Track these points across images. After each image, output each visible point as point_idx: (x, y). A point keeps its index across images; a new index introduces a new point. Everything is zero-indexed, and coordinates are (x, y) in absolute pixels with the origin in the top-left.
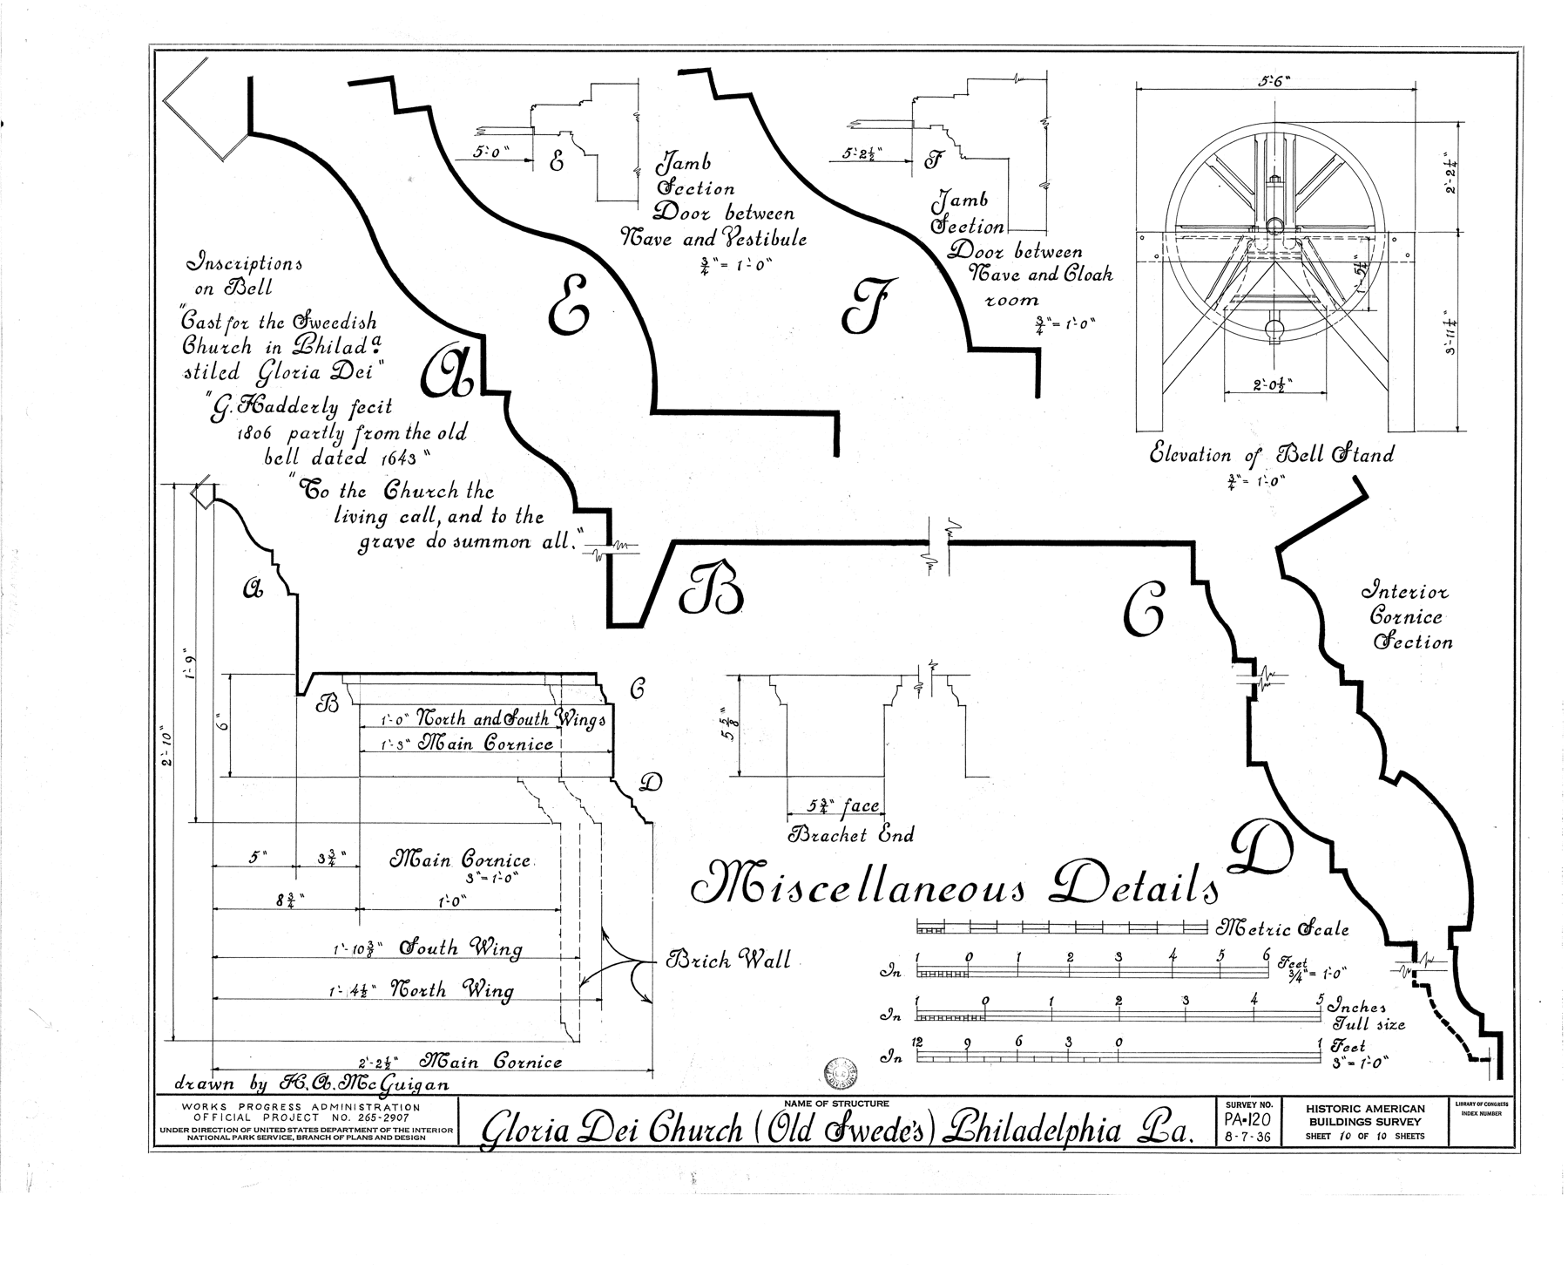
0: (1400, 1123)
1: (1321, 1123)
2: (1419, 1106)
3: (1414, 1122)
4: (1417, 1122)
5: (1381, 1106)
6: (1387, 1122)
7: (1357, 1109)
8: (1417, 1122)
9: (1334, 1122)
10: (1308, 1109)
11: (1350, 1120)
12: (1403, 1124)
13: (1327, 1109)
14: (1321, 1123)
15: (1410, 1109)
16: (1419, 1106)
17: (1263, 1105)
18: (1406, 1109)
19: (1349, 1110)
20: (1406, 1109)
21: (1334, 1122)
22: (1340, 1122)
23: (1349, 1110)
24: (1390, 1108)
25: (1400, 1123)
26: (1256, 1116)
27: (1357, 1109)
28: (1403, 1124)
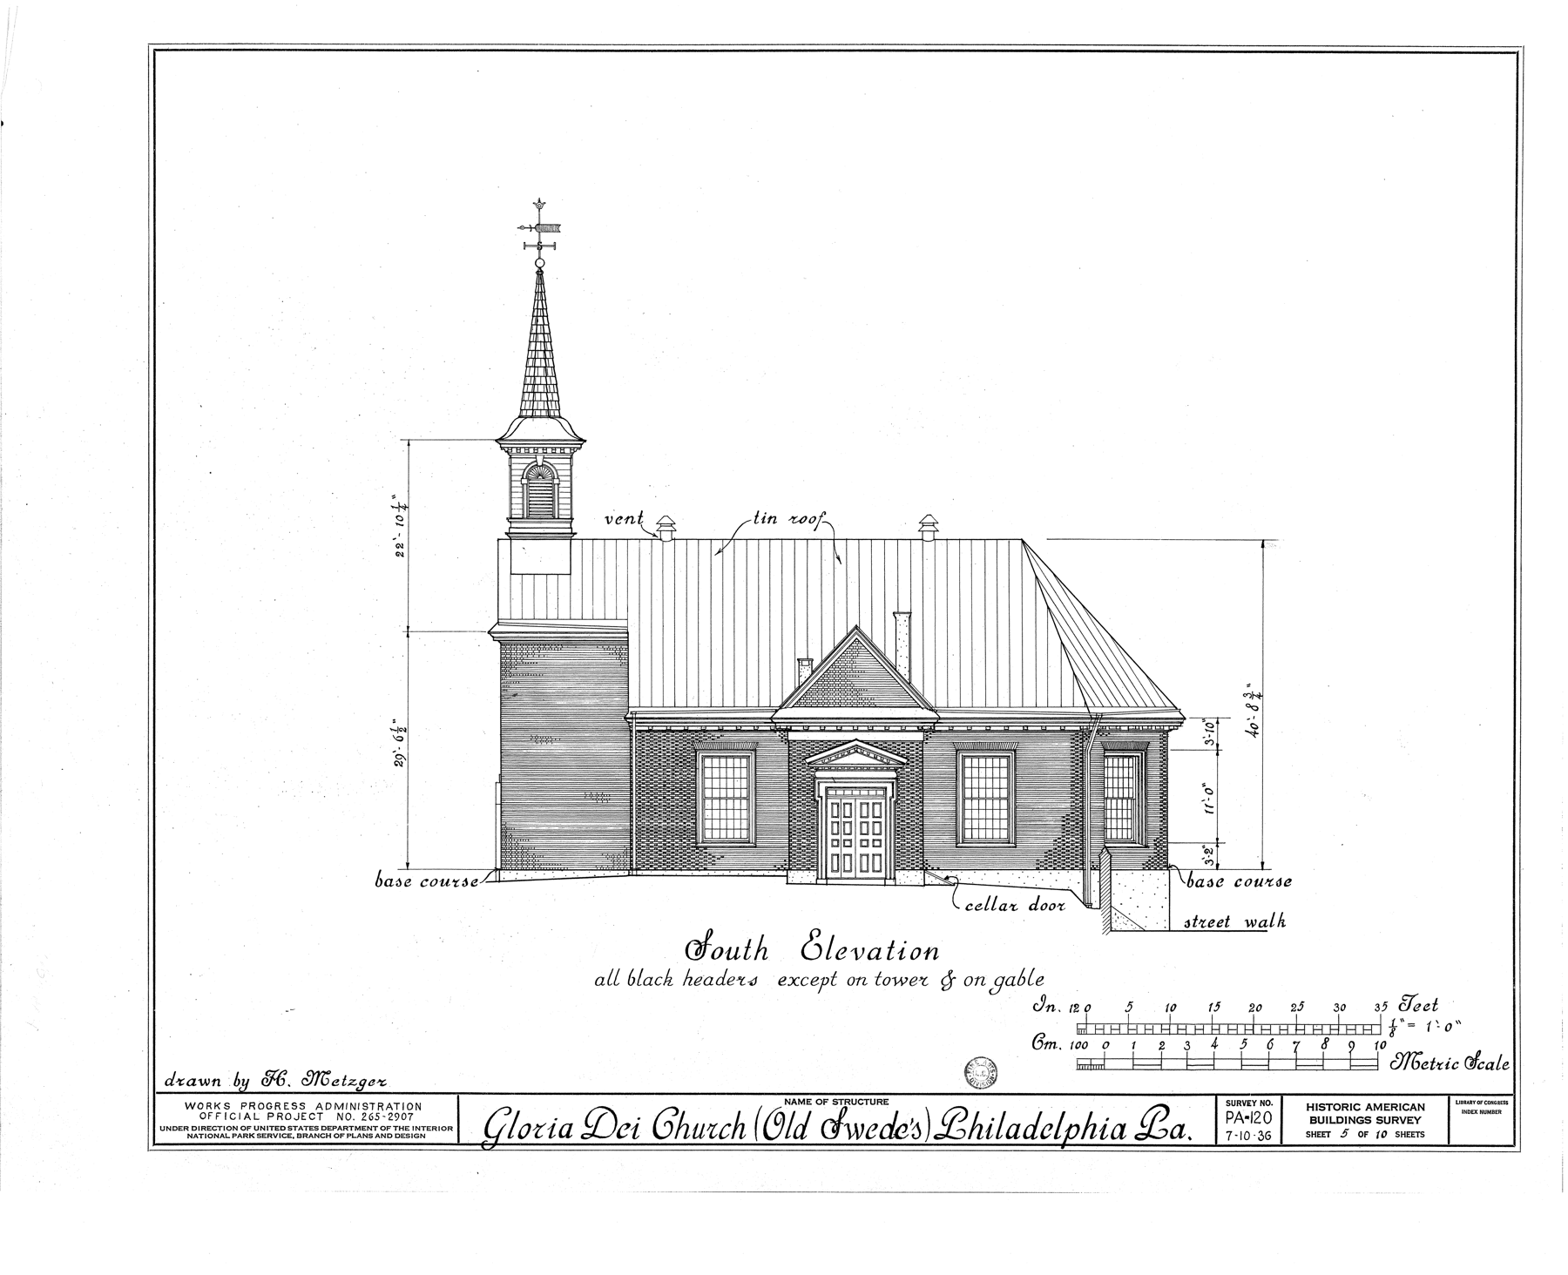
0: (1399, 1121)
1: (1321, 1121)
2: (1419, 1105)
3: (1414, 1120)
4: (1417, 1121)
5: (1381, 1105)
6: (1387, 1121)
7: (1357, 1107)
8: (1417, 1121)
9: (1334, 1120)
10: (1308, 1107)
11: (1350, 1118)
12: (1403, 1123)
13: (1327, 1107)
14: (1321, 1121)
15: (1410, 1107)
16: (1419, 1105)
17: (1263, 1103)
18: (1406, 1107)
19: (1349, 1108)
20: (1406, 1107)
21: (1334, 1120)
22: (1340, 1120)
23: (1349, 1108)
24: (1390, 1107)
25: (1399, 1121)
26: (1258, 1114)
27: (1357, 1107)
28: (1403, 1123)
